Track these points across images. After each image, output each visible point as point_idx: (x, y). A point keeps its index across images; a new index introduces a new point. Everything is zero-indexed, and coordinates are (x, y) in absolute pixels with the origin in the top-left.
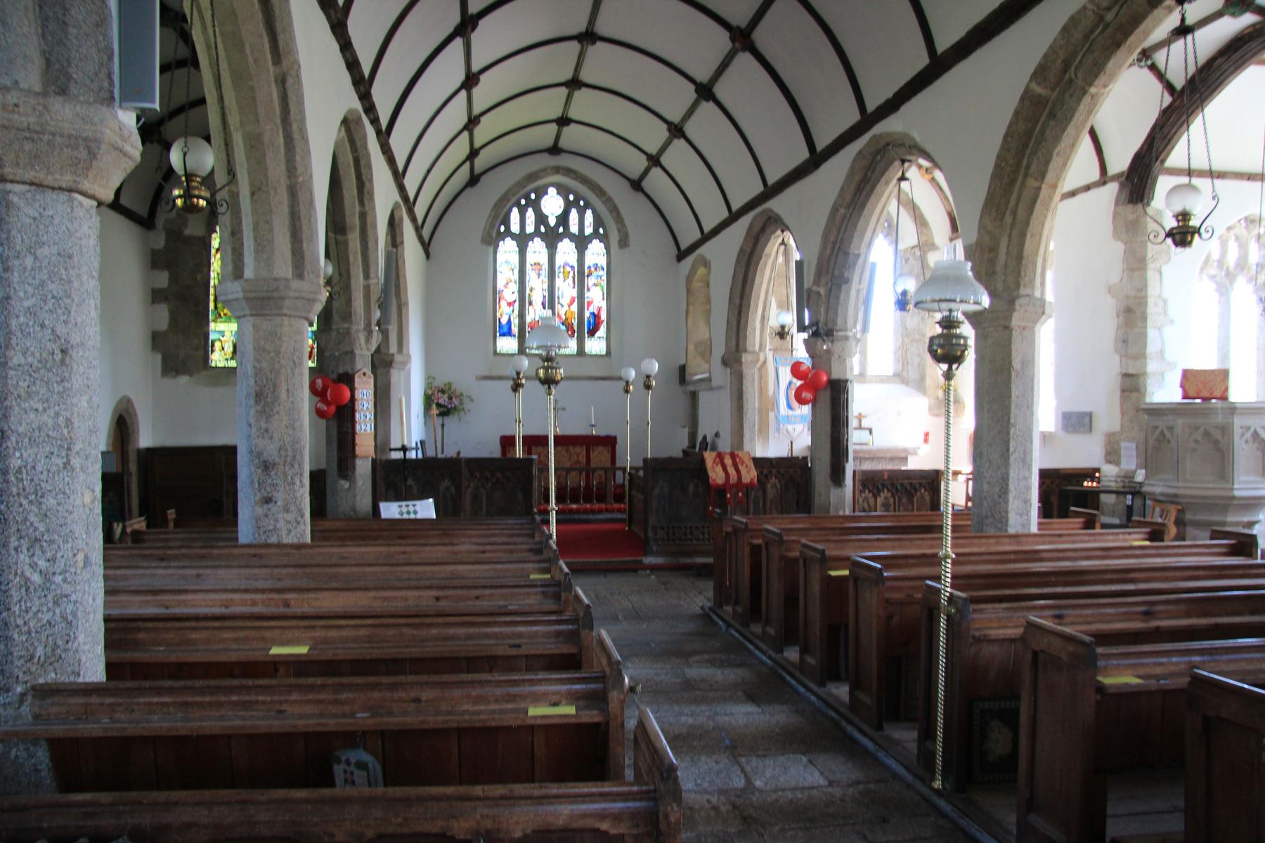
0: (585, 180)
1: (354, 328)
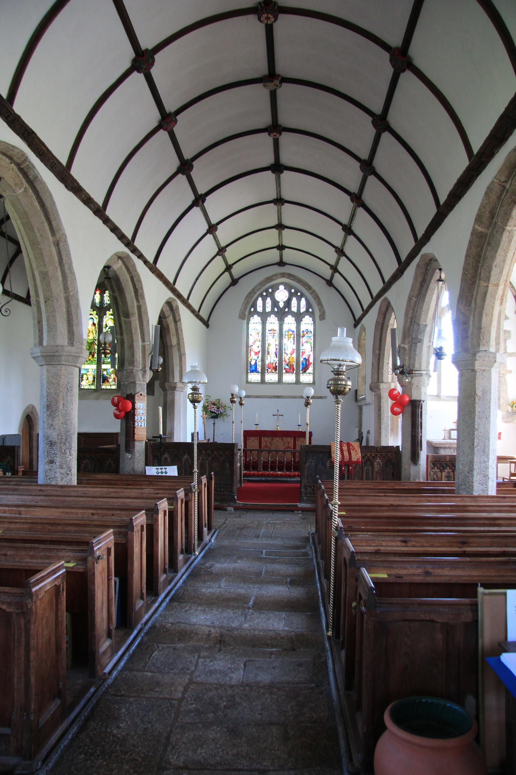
0: (299, 281)
1: (135, 369)
